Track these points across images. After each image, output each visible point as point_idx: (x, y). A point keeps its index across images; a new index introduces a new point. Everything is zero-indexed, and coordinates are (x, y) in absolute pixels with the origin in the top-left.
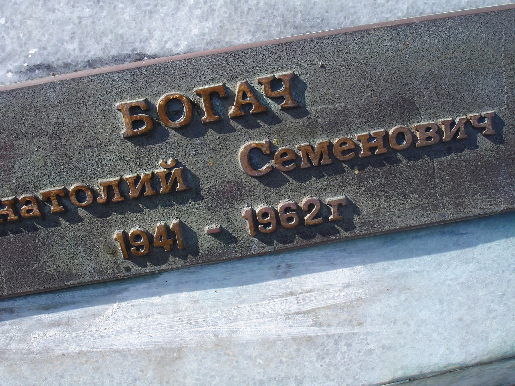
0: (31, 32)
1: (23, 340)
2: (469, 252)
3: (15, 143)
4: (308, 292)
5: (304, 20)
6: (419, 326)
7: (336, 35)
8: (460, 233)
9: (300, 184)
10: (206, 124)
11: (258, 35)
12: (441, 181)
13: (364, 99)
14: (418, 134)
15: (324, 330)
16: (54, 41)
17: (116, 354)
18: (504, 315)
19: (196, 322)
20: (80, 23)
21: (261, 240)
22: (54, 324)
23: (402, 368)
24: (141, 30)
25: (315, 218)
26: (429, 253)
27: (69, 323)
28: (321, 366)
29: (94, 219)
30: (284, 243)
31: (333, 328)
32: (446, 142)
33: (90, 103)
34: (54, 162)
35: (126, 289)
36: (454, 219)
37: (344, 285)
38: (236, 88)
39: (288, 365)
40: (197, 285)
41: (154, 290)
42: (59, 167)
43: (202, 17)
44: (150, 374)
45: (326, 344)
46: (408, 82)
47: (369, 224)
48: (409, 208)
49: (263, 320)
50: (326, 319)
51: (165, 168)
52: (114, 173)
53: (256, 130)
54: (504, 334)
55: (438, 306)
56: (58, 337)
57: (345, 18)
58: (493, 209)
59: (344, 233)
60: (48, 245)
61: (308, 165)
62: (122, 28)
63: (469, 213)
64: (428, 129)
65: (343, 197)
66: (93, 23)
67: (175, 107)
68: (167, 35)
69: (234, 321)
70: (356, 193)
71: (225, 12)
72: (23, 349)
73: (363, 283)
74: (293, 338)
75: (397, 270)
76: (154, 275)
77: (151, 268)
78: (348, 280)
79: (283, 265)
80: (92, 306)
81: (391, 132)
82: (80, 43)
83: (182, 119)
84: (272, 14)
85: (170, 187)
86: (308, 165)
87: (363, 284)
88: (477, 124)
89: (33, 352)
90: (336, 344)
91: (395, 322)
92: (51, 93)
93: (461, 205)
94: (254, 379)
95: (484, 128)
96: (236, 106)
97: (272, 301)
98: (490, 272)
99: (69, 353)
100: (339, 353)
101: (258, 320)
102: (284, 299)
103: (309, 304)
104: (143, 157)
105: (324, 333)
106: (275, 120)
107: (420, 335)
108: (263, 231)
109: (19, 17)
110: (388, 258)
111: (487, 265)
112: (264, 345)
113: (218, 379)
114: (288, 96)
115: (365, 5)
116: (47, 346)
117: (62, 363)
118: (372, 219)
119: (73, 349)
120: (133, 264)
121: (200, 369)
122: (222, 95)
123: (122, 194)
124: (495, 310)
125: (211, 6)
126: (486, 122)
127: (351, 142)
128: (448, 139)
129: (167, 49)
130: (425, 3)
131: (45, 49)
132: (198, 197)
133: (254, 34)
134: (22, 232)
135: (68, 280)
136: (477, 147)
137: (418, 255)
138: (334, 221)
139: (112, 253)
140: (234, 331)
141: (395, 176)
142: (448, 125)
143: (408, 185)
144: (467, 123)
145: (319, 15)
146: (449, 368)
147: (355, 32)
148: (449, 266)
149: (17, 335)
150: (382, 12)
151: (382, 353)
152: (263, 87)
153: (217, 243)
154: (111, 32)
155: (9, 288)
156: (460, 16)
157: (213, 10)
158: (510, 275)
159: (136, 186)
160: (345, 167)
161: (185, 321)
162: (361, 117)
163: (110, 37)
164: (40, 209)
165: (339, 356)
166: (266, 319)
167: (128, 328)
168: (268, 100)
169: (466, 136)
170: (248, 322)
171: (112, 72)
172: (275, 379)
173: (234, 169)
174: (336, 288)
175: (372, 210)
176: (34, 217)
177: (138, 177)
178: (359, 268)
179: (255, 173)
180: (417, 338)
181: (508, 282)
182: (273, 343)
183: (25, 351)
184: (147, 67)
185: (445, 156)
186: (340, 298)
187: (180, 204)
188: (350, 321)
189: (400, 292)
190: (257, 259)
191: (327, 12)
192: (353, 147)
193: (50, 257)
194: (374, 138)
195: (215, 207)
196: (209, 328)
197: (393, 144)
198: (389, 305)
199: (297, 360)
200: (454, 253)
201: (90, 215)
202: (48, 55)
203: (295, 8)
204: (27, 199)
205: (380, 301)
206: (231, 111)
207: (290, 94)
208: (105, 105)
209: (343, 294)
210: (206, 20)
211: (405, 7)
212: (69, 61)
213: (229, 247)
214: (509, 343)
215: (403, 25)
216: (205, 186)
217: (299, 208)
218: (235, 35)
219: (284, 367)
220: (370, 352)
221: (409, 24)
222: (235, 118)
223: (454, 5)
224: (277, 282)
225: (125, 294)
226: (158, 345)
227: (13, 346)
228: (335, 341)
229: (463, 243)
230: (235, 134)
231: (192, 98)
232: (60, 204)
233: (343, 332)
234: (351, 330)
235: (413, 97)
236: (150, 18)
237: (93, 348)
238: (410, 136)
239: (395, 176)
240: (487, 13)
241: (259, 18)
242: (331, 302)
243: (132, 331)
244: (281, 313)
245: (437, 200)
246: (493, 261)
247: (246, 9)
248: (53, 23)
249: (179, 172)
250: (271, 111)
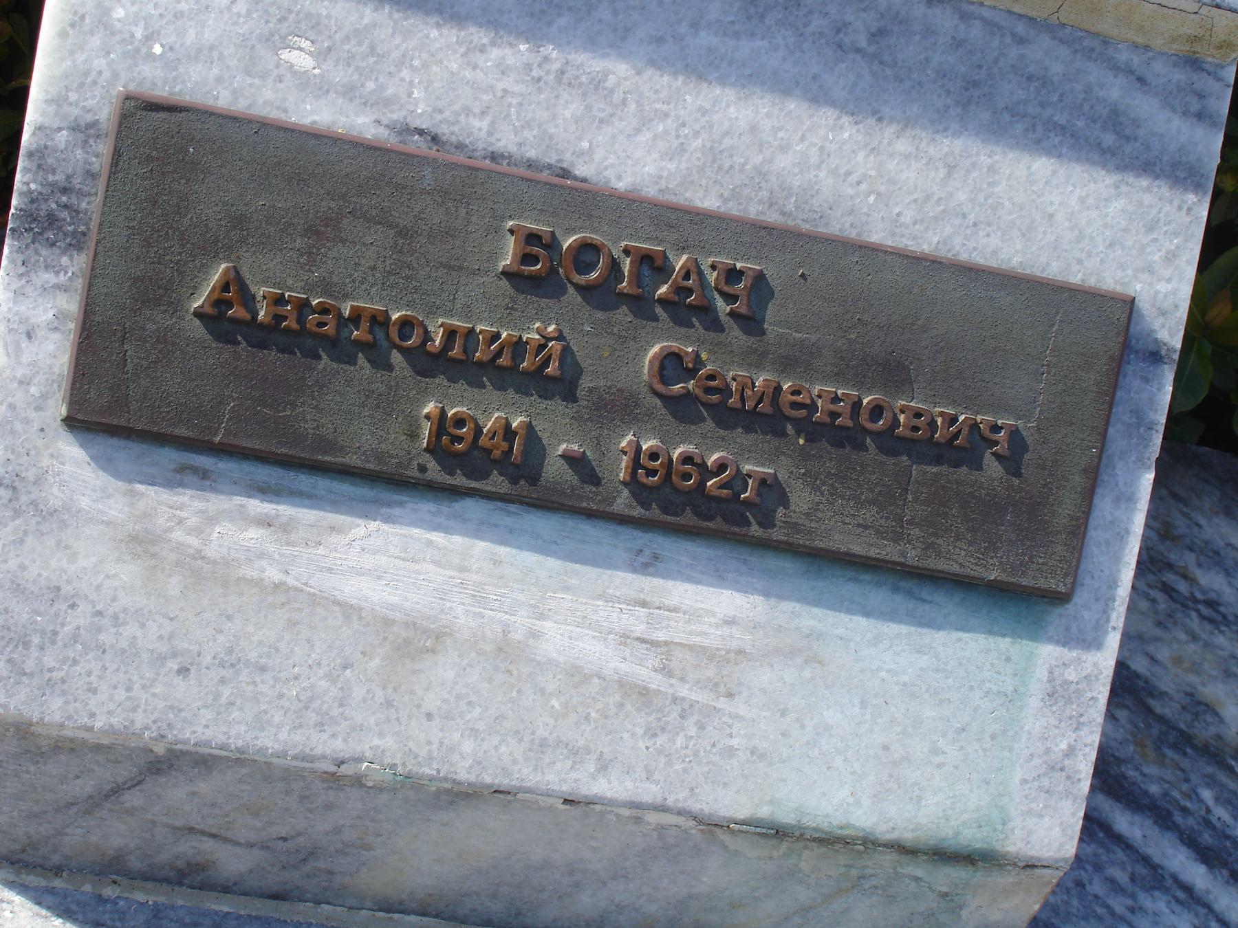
0: (432, 82)
1: (197, 531)
2: (929, 636)
3: (345, 221)
4: (669, 610)
5: (797, 207)
6: (818, 734)
7: (833, 241)
8: (921, 599)
9: (717, 429)
10: (621, 295)
11: (730, 204)
12: (916, 500)
13: (844, 340)
14: (902, 418)
15: (671, 685)
16: (457, 107)
17: (337, 609)
18: (956, 767)
19: (483, 597)
20: (503, 97)
21: (634, 495)
22: (266, 522)
23: (771, 802)
24: (580, 139)
25: (723, 486)
26: (867, 614)
27: (287, 527)
28: (647, 748)
29: (408, 372)
30: (667, 514)
31: (687, 686)
32: (938, 444)
33: (476, 208)
34: (387, 268)
35: (401, 504)
36: (918, 568)
37: (726, 618)
38: (680, 262)
39: (596, 728)
40: (508, 537)
41: (442, 520)
42: (392, 279)
43: (667, 153)
44: (375, 663)
45: (666, 710)
46: (910, 340)
47: (795, 527)
48: (859, 525)
49: (587, 632)
50: (681, 667)
52: (467, 316)
53: (684, 330)
54: (948, 802)
55: (857, 709)
56: (258, 545)
57: (851, 225)
58: (979, 572)
59: (755, 530)
60: (321, 388)
61: (739, 405)
62: (556, 126)
63: (942, 565)
64: (918, 415)
65: (772, 471)
66: (521, 104)
67: (588, 257)
68: (612, 159)
69: (541, 617)
70: (792, 472)
71: (699, 159)
72: (190, 547)
73: (756, 626)
74: (620, 682)
75: (812, 623)
76: (455, 493)
77: (459, 480)
78: (733, 613)
79: (648, 552)
80: (336, 513)
81: (865, 401)
82: (493, 123)
83: (594, 275)
84: (759, 184)
85: (537, 364)
86: (739, 405)
87: (754, 628)
88: (987, 433)
89: (203, 558)
90: (683, 717)
91: (783, 713)
92: (427, 172)
93: (934, 548)
94: (533, 733)
95: (996, 443)
96: (671, 286)
97: (610, 604)
98: (950, 681)
99: (262, 580)
100: (681, 735)
101: (579, 630)
102: (630, 607)
103: (664, 631)
104: (516, 310)
105: (670, 691)
106: (715, 325)
107: (817, 751)
108: (644, 480)
109: (425, 56)
110: (804, 600)
111: (949, 668)
112: (573, 676)
113: (478, 710)
114: (745, 298)
115: (882, 218)
116: (233, 554)
117: (241, 594)
118: (801, 522)
119: (273, 574)
120: (434, 462)
121: (456, 683)
122: (658, 263)
124: (943, 753)
125: (683, 144)
127: (808, 395)
128: (942, 441)
129: (605, 177)
130: (964, 245)
131: (441, 112)
132: (570, 396)
133: (726, 201)
134: (292, 353)
135: (325, 453)
136: (979, 468)
137: (849, 611)
138: (746, 502)
139: (411, 435)
140: (535, 635)
141: (853, 469)
142: (948, 419)
143: (867, 489)
144: (975, 426)
145: (819, 210)
146: (846, 832)
147: (860, 247)
148: (891, 647)
149: (193, 519)
150: (903, 236)
151: (748, 761)
152: (715, 274)
153: (570, 476)
154: (540, 126)
155: (228, 432)
156: (1004, 276)
157: (684, 150)
158: (981, 698)
160: (789, 428)
161: (466, 589)
162: (831, 364)
163: (535, 132)
164: (338, 329)
165: (680, 741)
166: (590, 632)
167: (375, 570)
168: (717, 296)
169: (968, 445)
170: (563, 627)
171: (523, 179)
172: (567, 744)
173: (634, 374)
174: (713, 620)
175: (806, 507)
176: (324, 337)
177: (497, 336)
178: (757, 599)
179: (660, 388)
180: (810, 753)
181: (976, 710)
182: (586, 679)
183: (191, 551)
184: (571, 188)
185: (931, 465)
186: (713, 637)
187: (540, 397)
188: (716, 685)
189: (806, 662)
191: (831, 209)
192: (808, 401)
193: (316, 407)
194: (842, 400)
195: (587, 420)
196: (499, 615)
197: (864, 419)
198: (783, 678)
199: (613, 723)
200: (904, 629)
201: (405, 364)
202: (441, 122)
203: (791, 188)
204: (327, 306)
205: (772, 666)
206: (663, 289)
207: (749, 296)
208: (494, 218)
209: (719, 633)
210: (670, 160)
211: (936, 239)
212: (467, 141)
213: (583, 488)
214: (952, 823)
215: (926, 260)
216: (586, 383)
217: (704, 463)
218: (701, 193)
219: (588, 729)
220: (730, 752)
221: (933, 262)
222: (663, 302)
223: (1002, 260)
224: (630, 576)
225: (396, 511)
226: (409, 615)
227: (178, 535)
228: (683, 710)
229: (922, 616)
230: (654, 324)
231: (615, 254)
232: (371, 331)
233: (700, 700)
234: (713, 700)
235: (911, 363)
236: (598, 128)
237: (305, 584)
238: (890, 415)
239: (853, 469)
240: (1043, 284)
241: (739, 183)
242: (697, 640)
243: (379, 578)
244: (617, 629)
245: (902, 527)
246: (960, 664)
247: (727, 165)
248: (467, 83)
250: (715, 311)
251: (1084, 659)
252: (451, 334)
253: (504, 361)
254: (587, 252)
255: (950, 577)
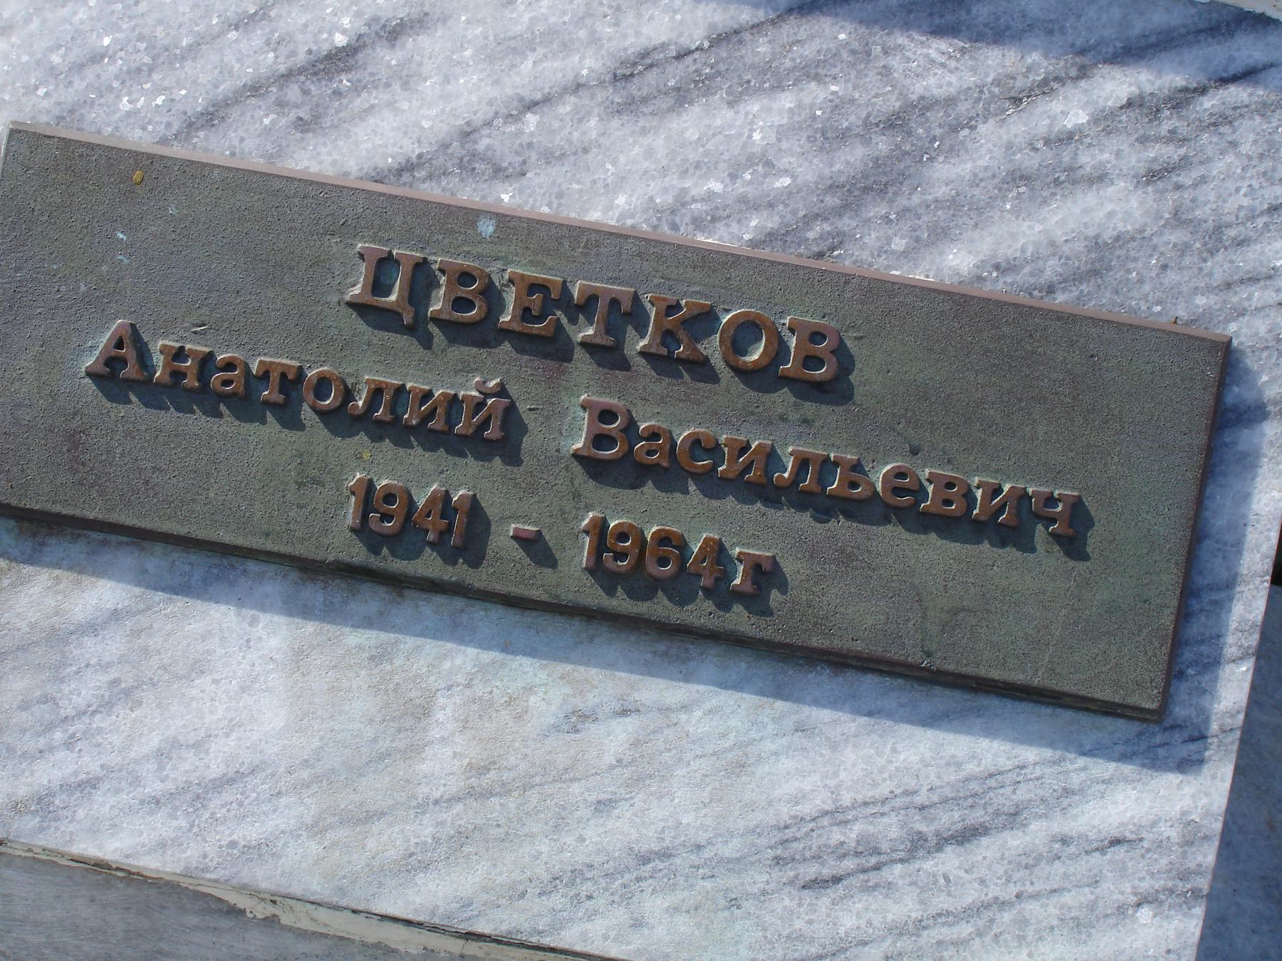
51: (480, 392)
64: (950, 485)
95: (1053, 520)
123: (393, 407)
126: (1059, 509)
128: (983, 518)
132: (513, 458)
144: (1024, 497)
159: (422, 404)
177: (997, 490)
190: (577, 623)
249: (501, 408)
251: (680, 919)
252: (803, 463)
253: (491, 433)
254: (748, 329)
255: (1045, 699)
